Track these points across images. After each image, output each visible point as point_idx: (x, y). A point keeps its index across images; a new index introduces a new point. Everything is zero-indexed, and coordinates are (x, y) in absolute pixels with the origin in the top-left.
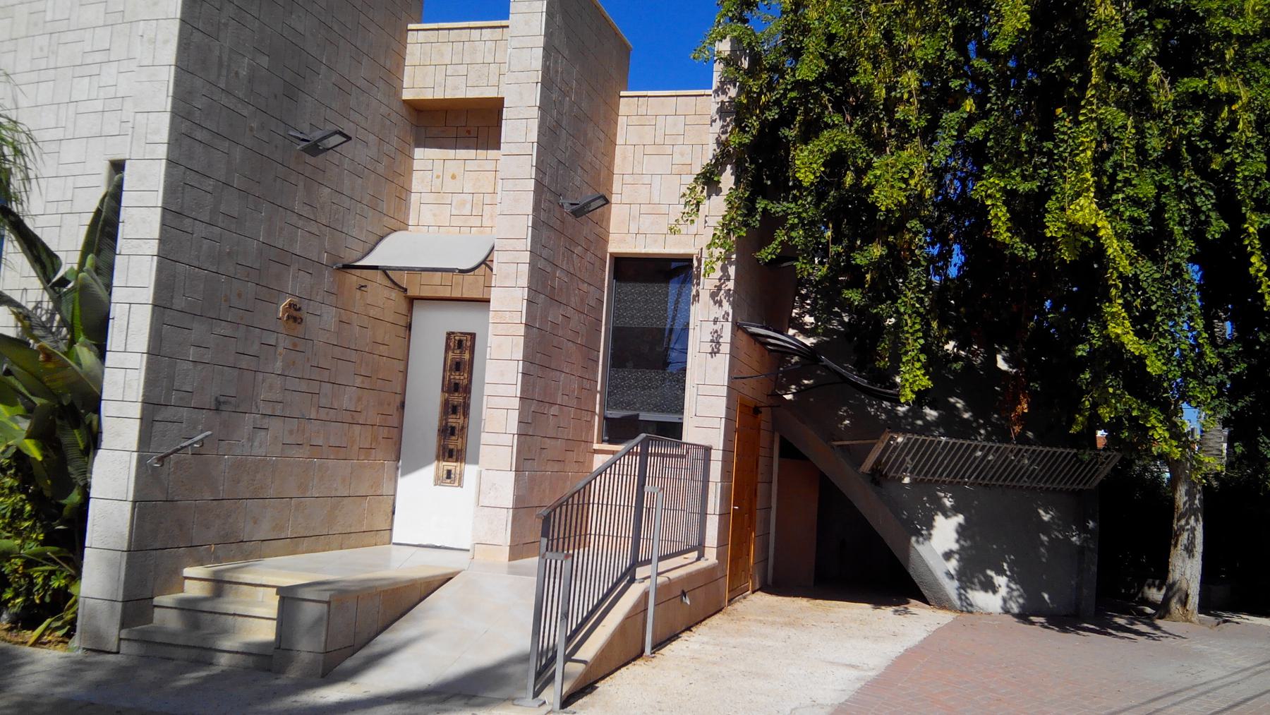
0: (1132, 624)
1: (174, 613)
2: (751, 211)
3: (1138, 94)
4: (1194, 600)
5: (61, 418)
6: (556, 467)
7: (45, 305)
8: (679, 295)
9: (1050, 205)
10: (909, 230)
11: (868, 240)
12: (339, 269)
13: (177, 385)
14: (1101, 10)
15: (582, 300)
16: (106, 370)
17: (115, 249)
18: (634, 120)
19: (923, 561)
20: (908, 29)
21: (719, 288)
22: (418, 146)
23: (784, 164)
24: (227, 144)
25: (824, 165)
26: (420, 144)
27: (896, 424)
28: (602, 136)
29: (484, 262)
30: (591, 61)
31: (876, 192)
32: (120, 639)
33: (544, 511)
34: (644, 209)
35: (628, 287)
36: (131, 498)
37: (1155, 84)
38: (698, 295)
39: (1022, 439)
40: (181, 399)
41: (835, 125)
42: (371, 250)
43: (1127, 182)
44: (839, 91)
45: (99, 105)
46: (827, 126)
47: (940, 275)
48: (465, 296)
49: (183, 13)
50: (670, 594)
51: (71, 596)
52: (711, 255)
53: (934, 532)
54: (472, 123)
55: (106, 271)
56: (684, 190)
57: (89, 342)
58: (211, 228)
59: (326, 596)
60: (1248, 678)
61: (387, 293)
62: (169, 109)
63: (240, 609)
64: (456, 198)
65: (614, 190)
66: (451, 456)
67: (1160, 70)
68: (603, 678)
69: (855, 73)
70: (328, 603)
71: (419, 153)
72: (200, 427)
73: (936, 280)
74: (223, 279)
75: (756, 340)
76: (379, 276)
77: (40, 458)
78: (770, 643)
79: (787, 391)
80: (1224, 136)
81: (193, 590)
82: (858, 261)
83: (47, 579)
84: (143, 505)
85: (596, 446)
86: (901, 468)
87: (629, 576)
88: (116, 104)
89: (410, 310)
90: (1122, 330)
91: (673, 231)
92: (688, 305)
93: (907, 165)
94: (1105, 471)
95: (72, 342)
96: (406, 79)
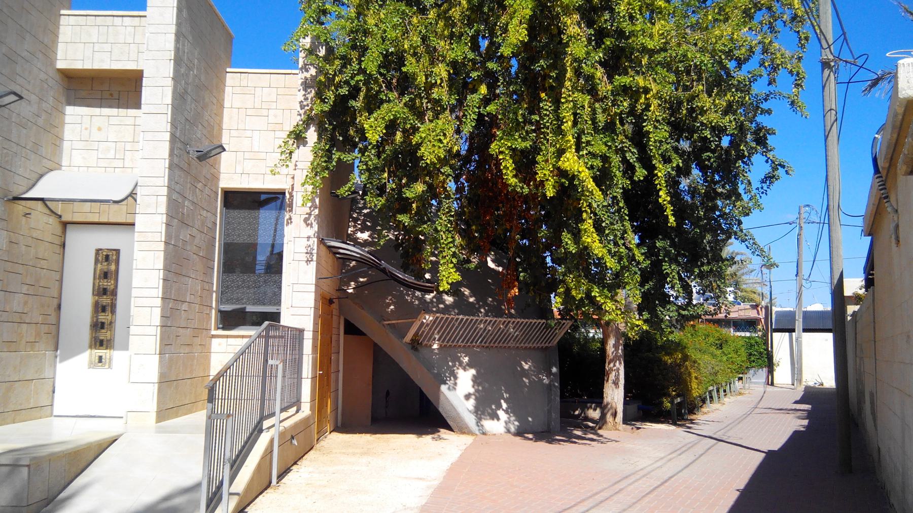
2: (330, 159)
4: (620, 415)
6: (187, 349)
10: (443, 174)
12: (9, 200)
14: (571, 29)
15: (203, 224)
18: (238, 90)
22: (69, 104)
26: (69, 104)
28: (215, 101)
31: (423, 149)
34: (247, 155)
35: (235, 213)
38: (290, 219)
42: (34, 185)
43: (588, 143)
48: (112, 220)
50: (287, 437)
53: (458, 381)
54: (117, 89)
60: (665, 464)
67: (602, 70)
68: (248, 505)
71: (69, 110)
80: (641, 114)
82: (407, 195)
85: (214, 332)
87: (258, 430)
90: (591, 239)
93: (442, 130)
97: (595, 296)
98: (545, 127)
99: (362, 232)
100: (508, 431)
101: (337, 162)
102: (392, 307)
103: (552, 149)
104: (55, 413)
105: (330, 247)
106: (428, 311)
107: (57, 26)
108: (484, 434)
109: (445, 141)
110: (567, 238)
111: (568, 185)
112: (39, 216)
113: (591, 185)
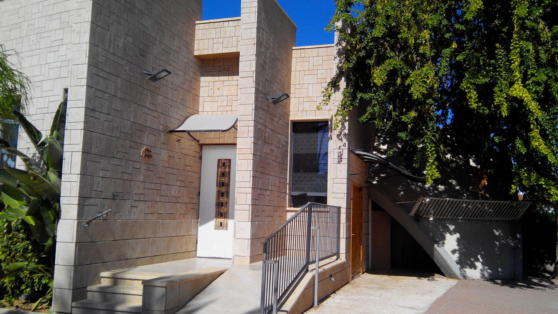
0: (541, 282)
1: (97, 294)
5: (42, 206)
6: (270, 219)
8: (322, 138)
9: (496, 89)
11: (409, 110)
12: (167, 132)
13: (94, 188)
16: (62, 183)
17: (64, 127)
20: (424, 12)
21: (341, 133)
22: (202, 76)
24: (114, 77)
25: (387, 76)
26: (203, 75)
27: (425, 193)
28: (285, 67)
29: (233, 126)
30: (279, 34)
32: (72, 307)
33: (263, 240)
34: (305, 99)
35: (299, 135)
36: (75, 241)
37: (541, 29)
41: (391, 57)
42: (182, 123)
43: (533, 75)
44: (392, 41)
46: (388, 58)
47: (442, 123)
48: (226, 142)
49: (92, 19)
50: (324, 276)
51: (49, 287)
52: (337, 120)
53: (445, 242)
54: (226, 64)
55: (60, 138)
56: (323, 90)
58: (108, 116)
59: (165, 284)
61: (190, 142)
62: (87, 62)
66: (222, 216)
67: (543, 23)
69: (399, 33)
70: (166, 287)
71: (202, 79)
72: (106, 207)
73: (441, 127)
74: (114, 139)
75: (359, 157)
76: (186, 135)
77: (34, 225)
78: (372, 298)
79: (374, 180)
81: (105, 283)
83: (40, 279)
84: (80, 244)
85: (288, 209)
86: (429, 213)
87: (305, 269)
89: (201, 150)
90: (538, 143)
91: (318, 108)
93: (425, 74)
94: (523, 211)
95: (48, 170)
97: (542, 185)
98: (500, 67)
99: (384, 145)
100: (483, 276)
105: (358, 155)
107: (194, 30)
108: (465, 277)
109: (428, 82)
110: (518, 143)
111: (517, 105)
112: (186, 142)
113: (533, 106)
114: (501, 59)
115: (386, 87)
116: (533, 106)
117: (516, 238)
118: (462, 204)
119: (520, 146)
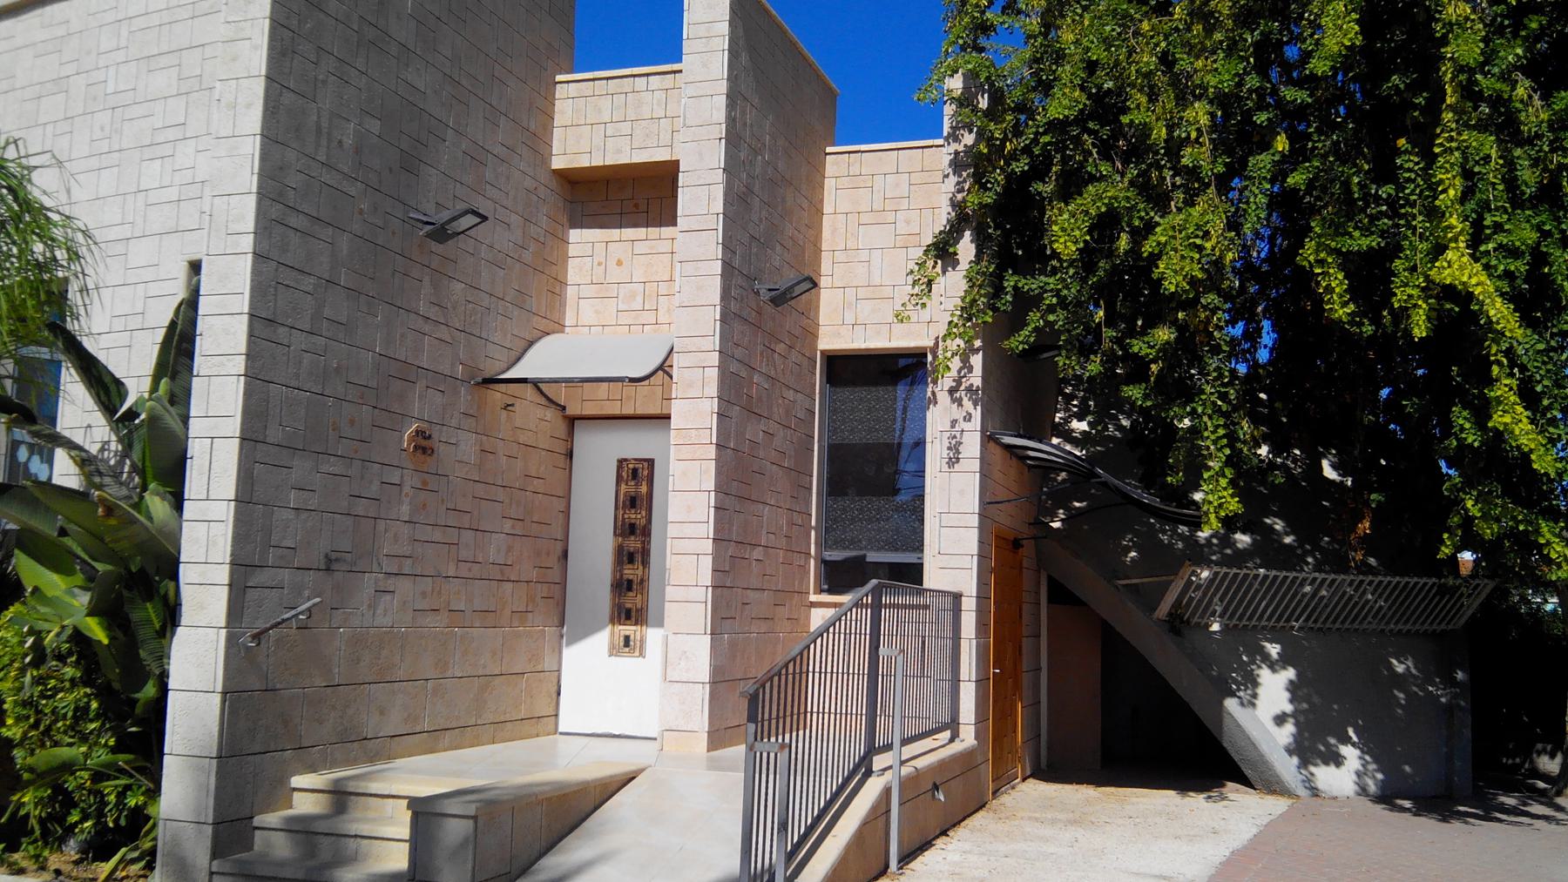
0: (1525, 804)
2: (998, 291)
3: (1501, 114)
5: (130, 589)
7: (113, 446)
11: (1151, 324)
12: (478, 384)
13: (274, 540)
14: (1451, 10)
15: (787, 412)
18: (844, 182)
19: (1243, 731)
20: (1195, 51)
23: (1039, 229)
27: (1198, 554)
28: (805, 205)
29: (661, 368)
30: (789, 108)
32: (212, 873)
33: (750, 687)
34: (862, 293)
36: (219, 688)
37: (1522, 101)
39: (1364, 568)
40: (282, 557)
41: (1102, 178)
42: (519, 359)
43: (1498, 228)
44: (1105, 132)
45: (173, 194)
46: (1093, 179)
47: (1246, 361)
48: (639, 412)
50: (918, 788)
51: (148, 818)
52: (945, 350)
53: (1260, 691)
54: (641, 194)
55: (180, 399)
56: (912, 265)
57: (161, 489)
59: (471, 810)
63: (365, 829)
64: (624, 289)
65: (823, 272)
66: (628, 617)
67: (1527, 83)
69: (1125, 110)
70: (475, 818)
71: (575, 235)
72: (306, 593)
73: (1242, 369)
75: (1012, 454)
76: (529, 391)
77: (106, 641)
78: (1052, 849)
79: (1053, 515)
81: (305, 805)
83: (121, 795)
84: (235, 697)
85: (813, 598)
86: (1208, 613)
87: (864, 769)
88: (194, 191)
89: (571, 433)
90: (1513, 420)
91: (900, 318)
92: (924, 409)
94: (1471, 606)
95: (144, 488)
96: (556, 144)
99: (1080, 420)
100: (1363, 791)
101: (1014, 296)
102: (1133, 554)
103: (1424, 246)
104: (561, 729)
106: (1205, 562)
108: (1315, 792)
109: (1208, 245)
110: (1461, 418)
111: (1456, 308)
113: (1499, 311)
114: (1413, 181)
115: (1087, 258)
116: (1499, 311)
117: (1452, 682)
118: (1302, 585)
119: (1467, 425)
